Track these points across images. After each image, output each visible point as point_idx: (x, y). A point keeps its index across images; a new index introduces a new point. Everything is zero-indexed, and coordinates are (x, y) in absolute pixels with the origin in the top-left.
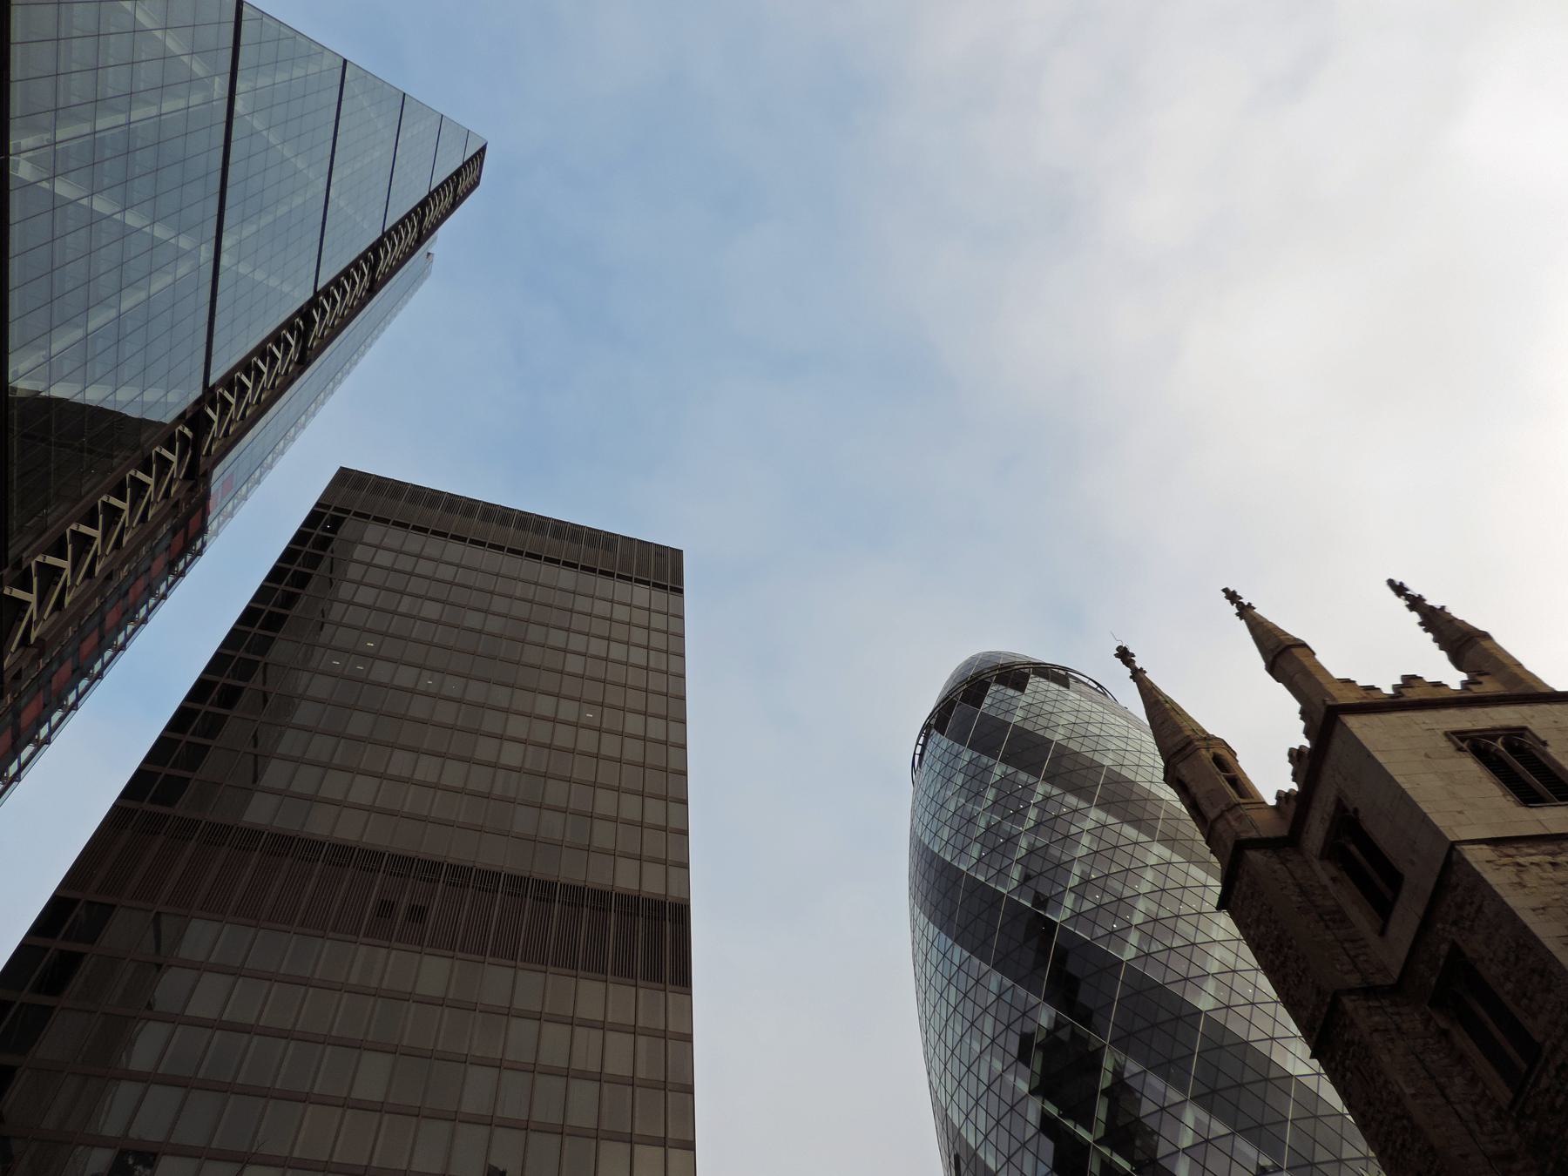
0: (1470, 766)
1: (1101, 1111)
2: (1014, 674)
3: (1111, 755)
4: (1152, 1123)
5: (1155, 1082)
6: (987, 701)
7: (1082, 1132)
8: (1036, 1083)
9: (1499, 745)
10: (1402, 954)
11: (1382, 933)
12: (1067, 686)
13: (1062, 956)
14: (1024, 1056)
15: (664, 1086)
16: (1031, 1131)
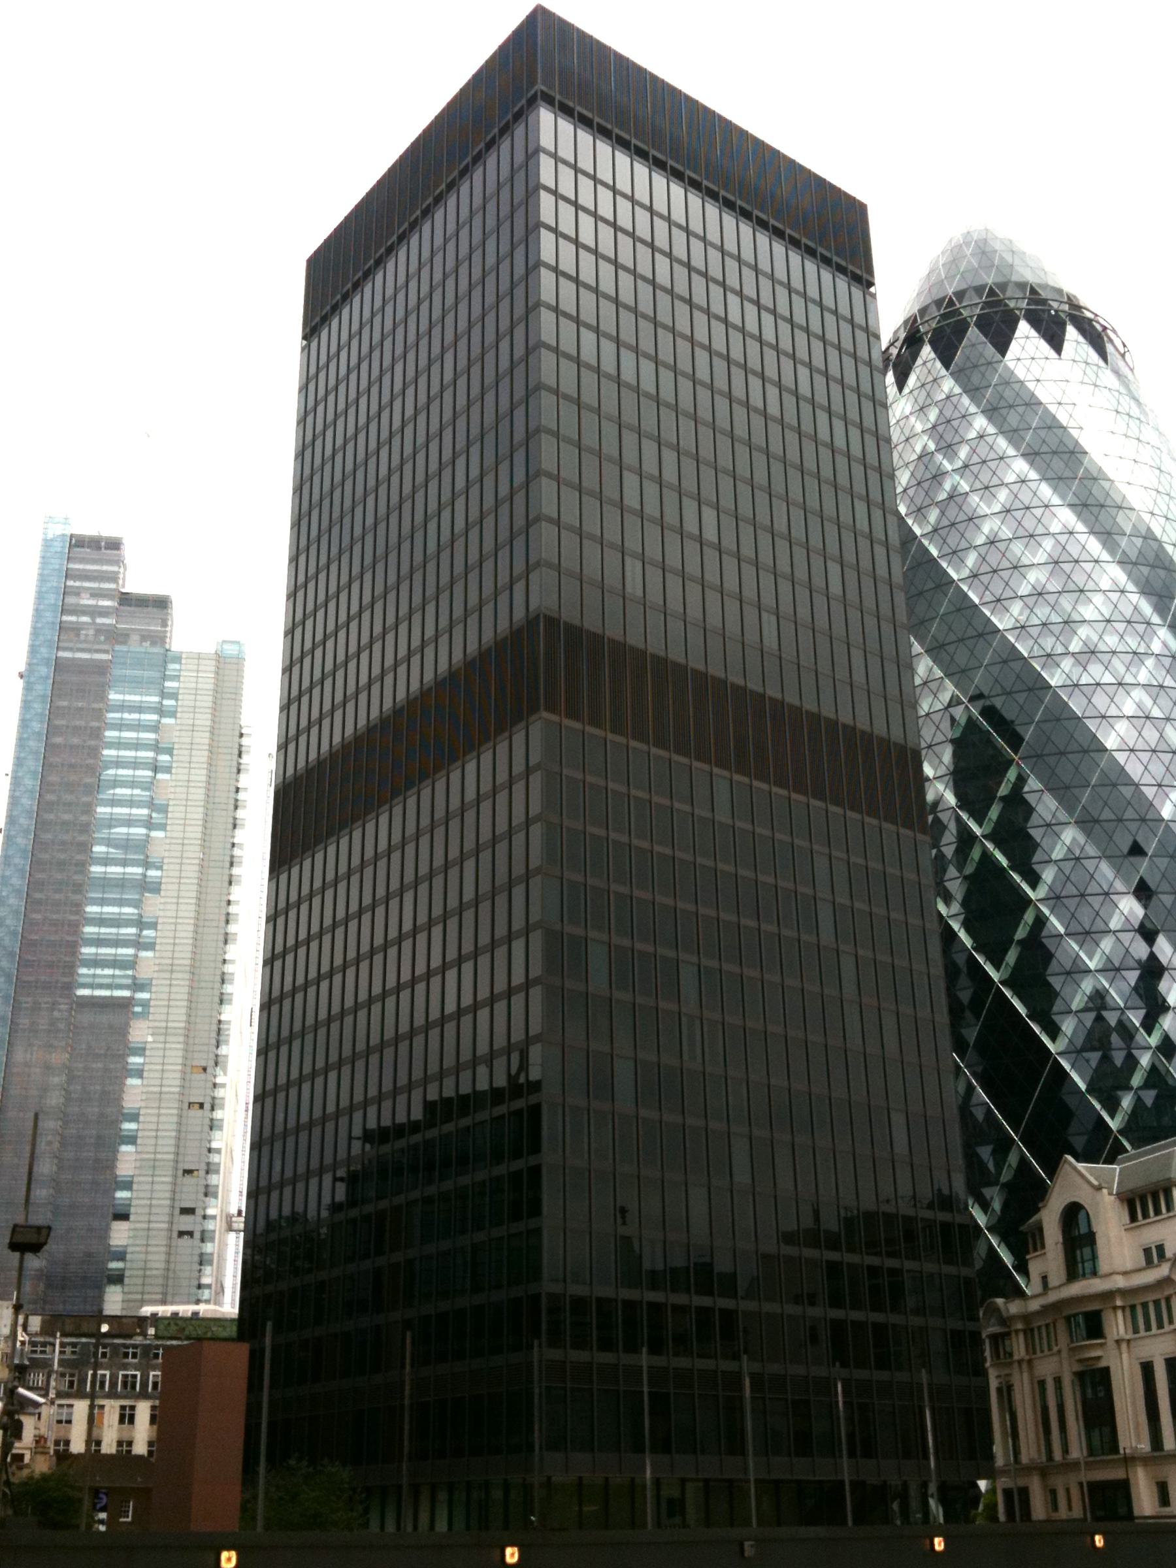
7: (989, 969)
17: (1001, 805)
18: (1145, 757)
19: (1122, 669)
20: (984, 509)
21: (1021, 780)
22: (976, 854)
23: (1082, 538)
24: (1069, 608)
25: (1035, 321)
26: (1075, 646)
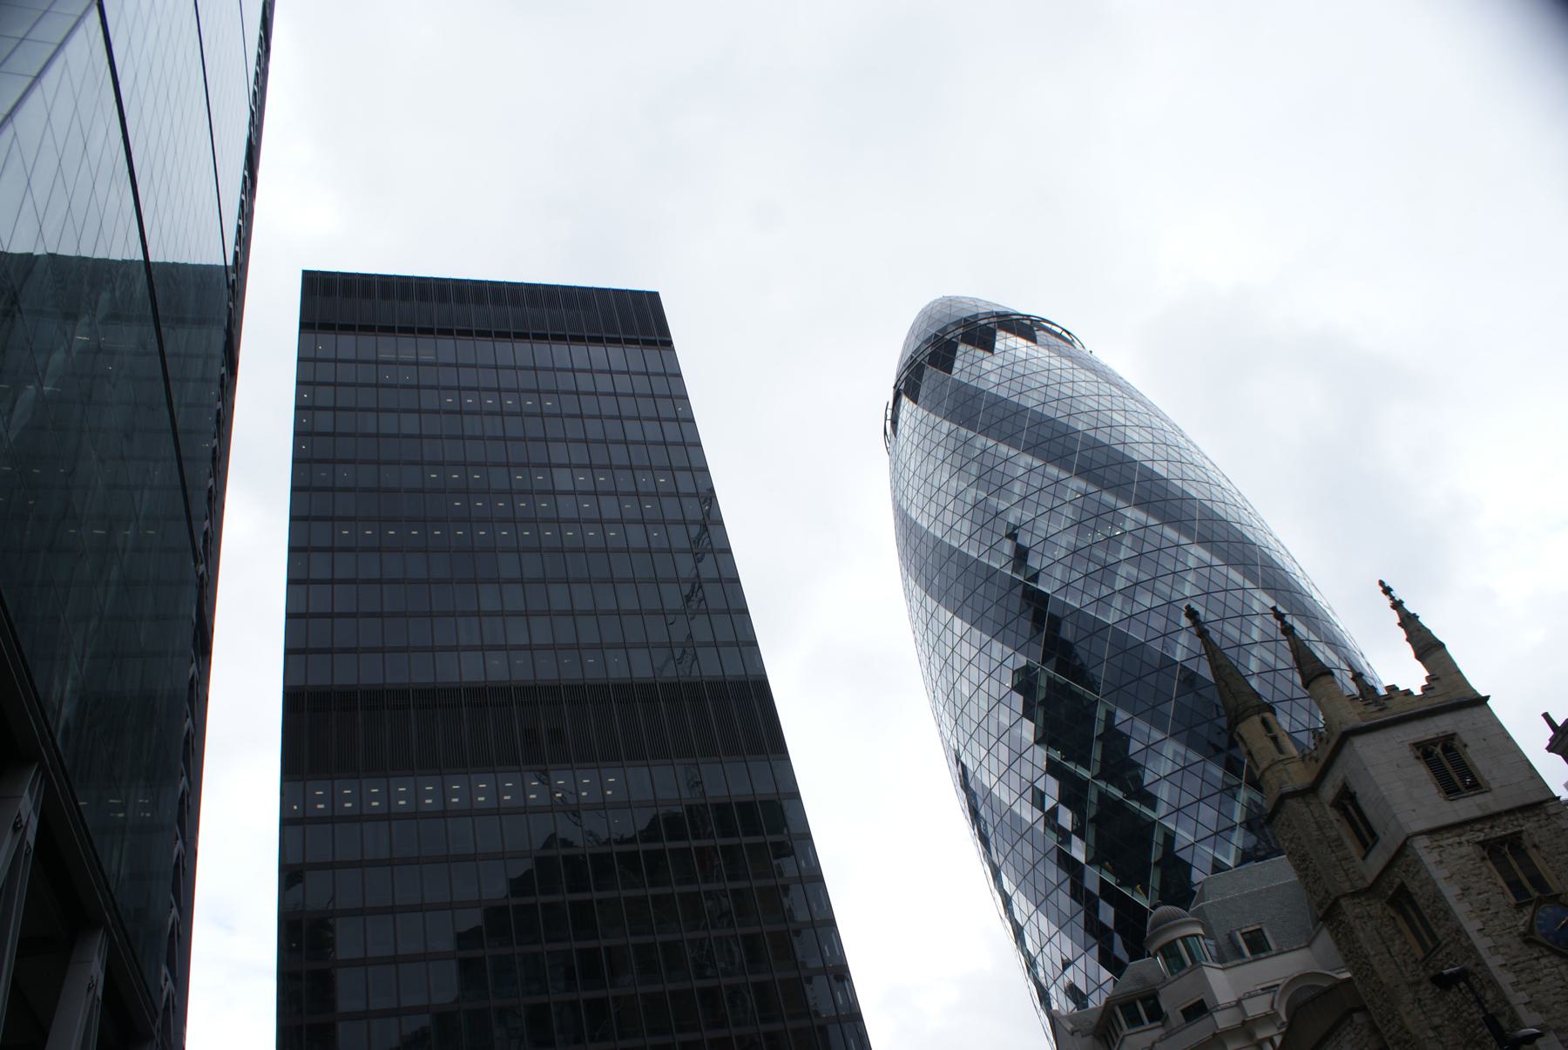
0: (1422, 771)
1: (1097, 753)
2: (981, 330)
4: (1138, 759)
5: (1141, 725)
6: (958, 364)
9: (1438, 750)
10: (1376, 873)
11: (1364, 858)
12: (1033, 339)
13: (1056, 622)
16: (1038, 773)
19: (1167, 590)
20: (1003, 505)
21: (1110, 715)
22: (1093, 796)
23: (1158, 529)
24: (1167, 590)
25: (969, 339)
26: (1120, 584)
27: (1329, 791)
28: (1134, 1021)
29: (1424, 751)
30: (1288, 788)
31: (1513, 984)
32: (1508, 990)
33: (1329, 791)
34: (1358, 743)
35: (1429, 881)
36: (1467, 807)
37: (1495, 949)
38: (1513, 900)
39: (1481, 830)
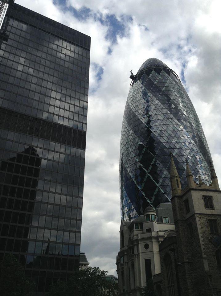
1: (150, 168)
3: (168, 81)
6: (151, 75)
7: (149, 201)
8: (140, 160)
11: (186, 214)
14: (139, 155)
15: (83, 115)
17: (151, 166)
18: (176, 99)
21: (156, 161)
22: (146, 177)
25: (155, 70)
27: (184, 199)
28: (137, 228)
29: (205, 198)
30: (177, 195)
31: (204, 248)
32: (202, 249)
33: (184, 199)
34: (192, 191)
35: (196, 224)
36: (209, 211)
37: (203, 241)
38: (210, 232)
39: (209, 217)
